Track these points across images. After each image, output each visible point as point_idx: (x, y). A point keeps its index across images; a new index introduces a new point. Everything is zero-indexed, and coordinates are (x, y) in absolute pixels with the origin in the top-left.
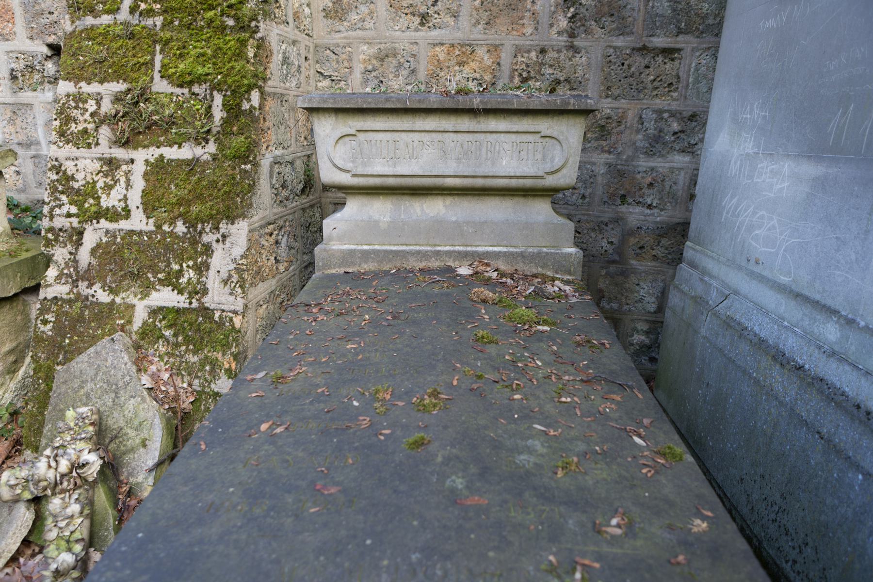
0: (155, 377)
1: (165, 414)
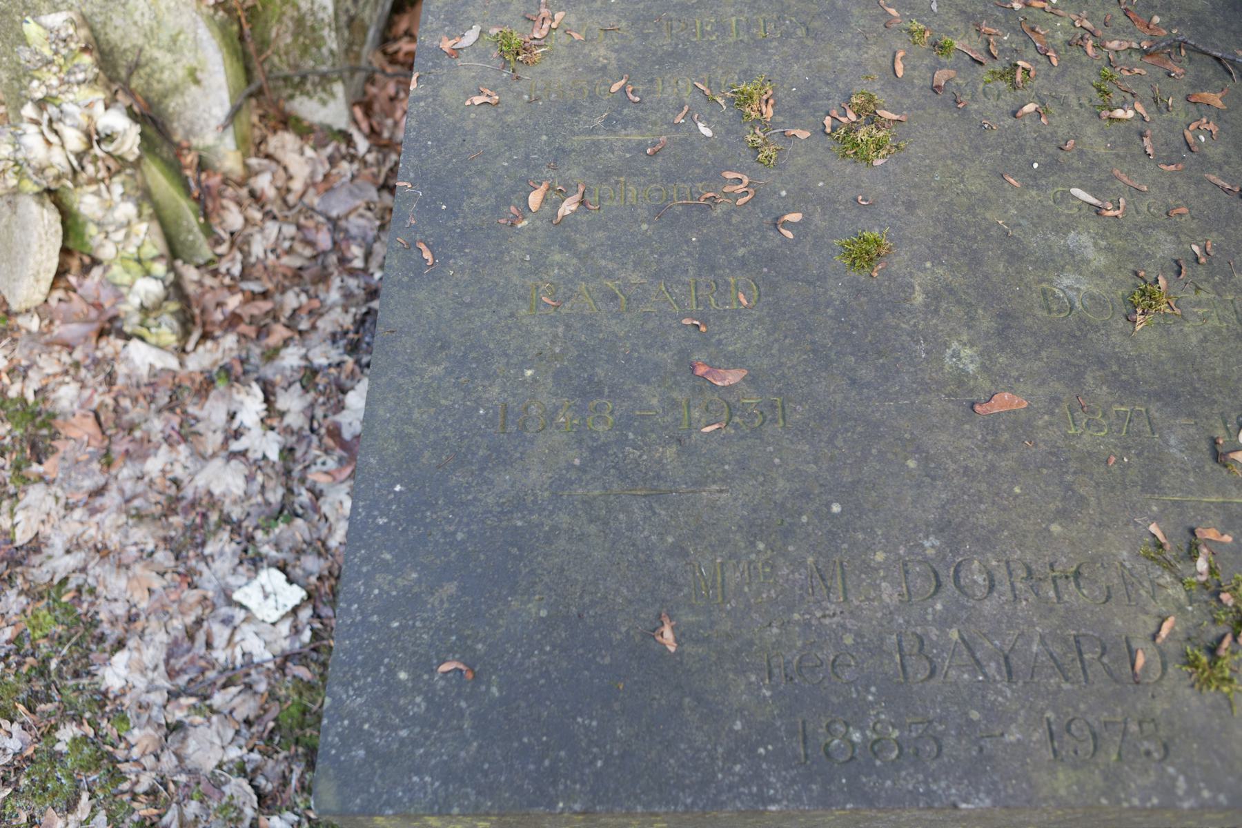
1: (212, 17)
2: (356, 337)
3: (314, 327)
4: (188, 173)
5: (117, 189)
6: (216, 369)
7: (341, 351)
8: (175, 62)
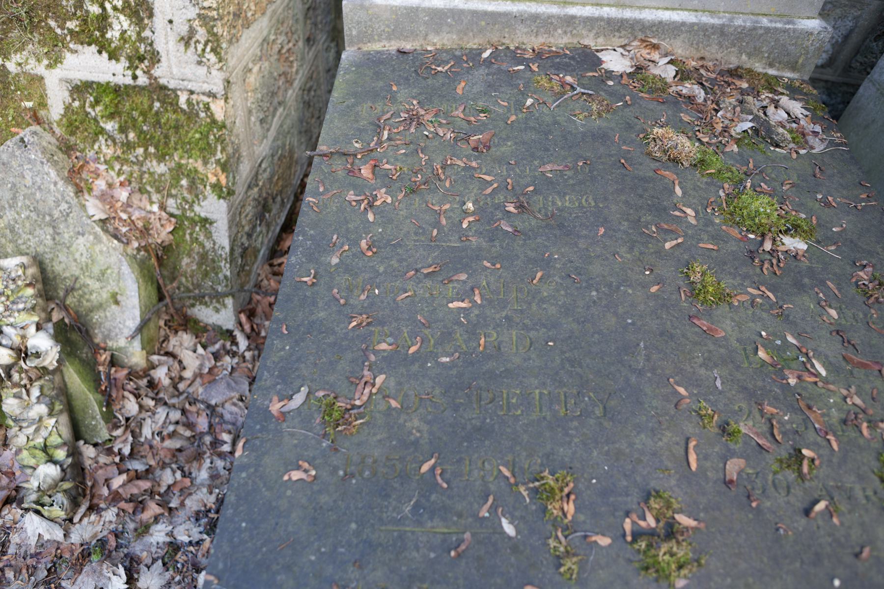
0: (106, 198)
1: (135, 257)
2: (216, 516)
3: (182, 504)
4: (101, 368)
5: (35, 392)
6: (94, 542)
7: (201, 529)
8: (101, 288)
